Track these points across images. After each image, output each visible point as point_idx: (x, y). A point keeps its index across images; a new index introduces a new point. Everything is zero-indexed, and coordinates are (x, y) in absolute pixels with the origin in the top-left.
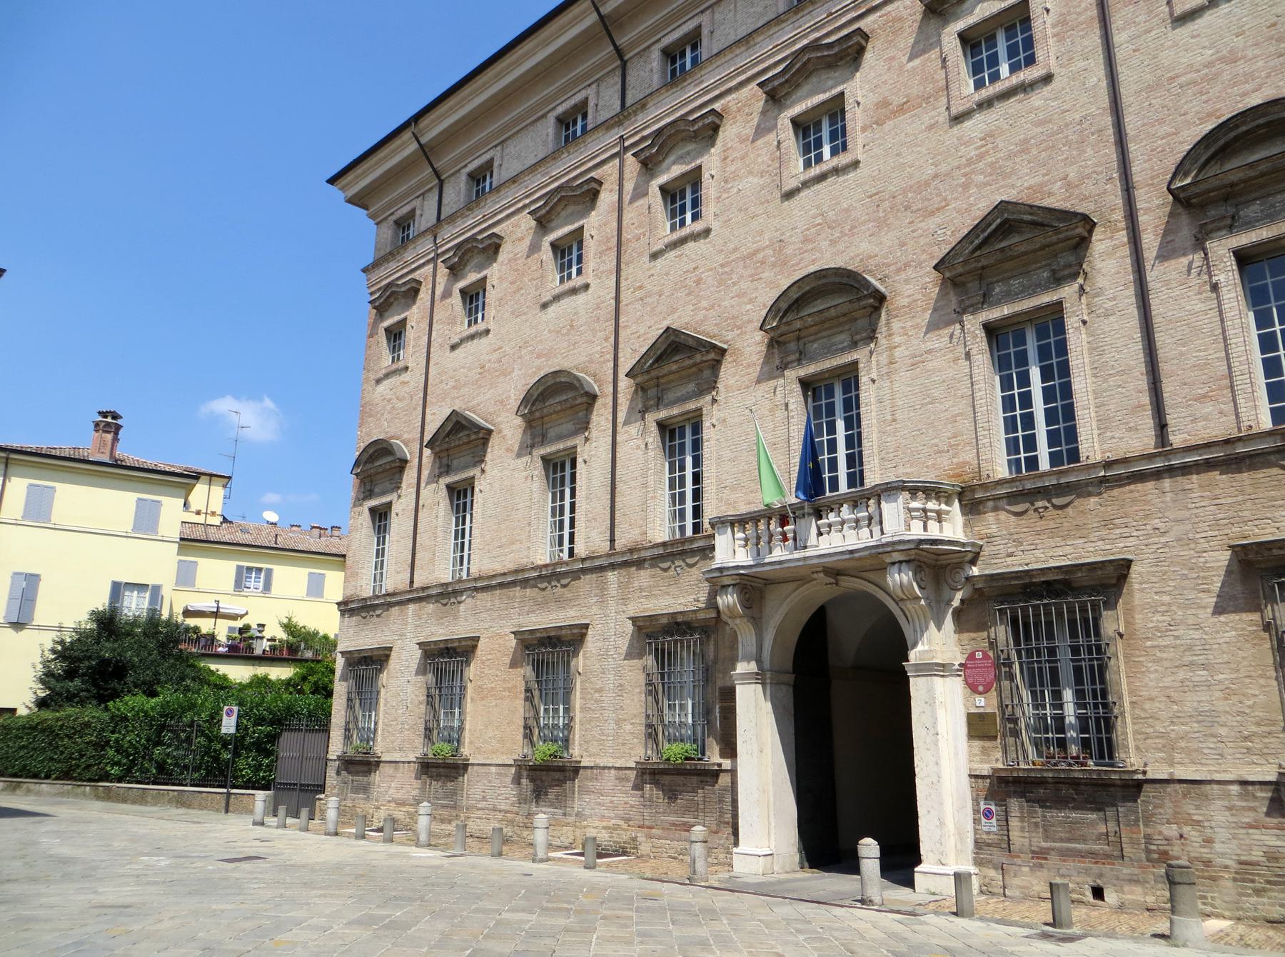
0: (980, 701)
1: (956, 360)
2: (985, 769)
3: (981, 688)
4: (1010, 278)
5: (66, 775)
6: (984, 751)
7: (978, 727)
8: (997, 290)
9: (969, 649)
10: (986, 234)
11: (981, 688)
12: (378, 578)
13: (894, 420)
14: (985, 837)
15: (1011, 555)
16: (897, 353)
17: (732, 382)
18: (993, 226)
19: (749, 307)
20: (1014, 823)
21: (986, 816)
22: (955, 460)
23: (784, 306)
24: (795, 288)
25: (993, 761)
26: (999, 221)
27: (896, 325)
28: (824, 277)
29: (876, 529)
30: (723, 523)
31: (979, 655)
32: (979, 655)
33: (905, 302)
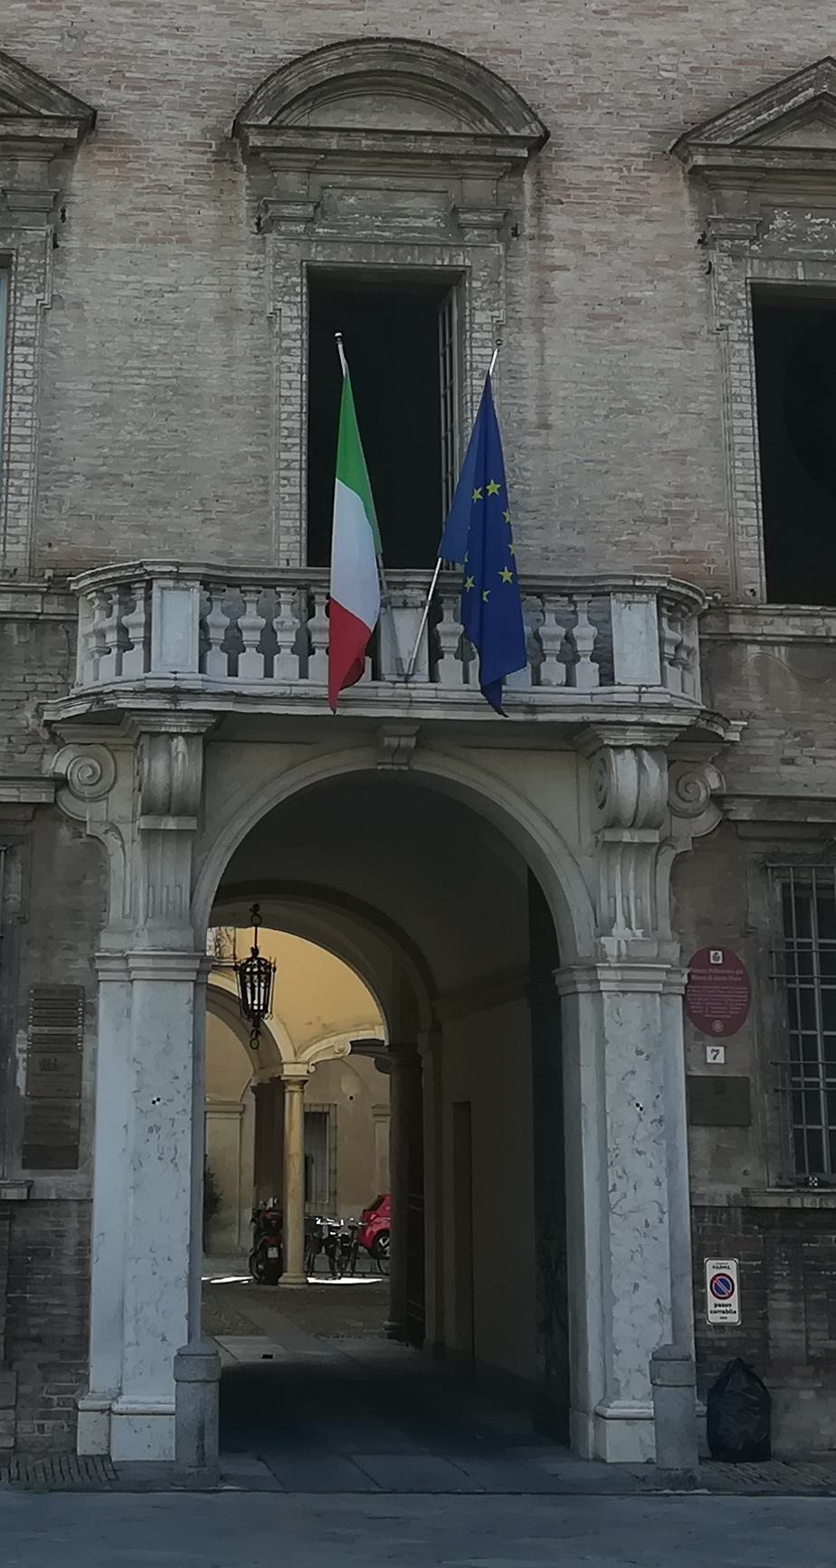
0: (716, 1055)
1: (689, 337)
2: (720, 1193)
3: (718, 1026)
4: (806, 207)
5: (769, 1413)
6: (720, 1159)
7: (711, 1101)
8: (779, 223)
9: (694, 945)
10: (785, 108)
11: (718, 1026)
12: (445, 634)
13: (546, 426)
14: (710, 1335)
15: (791, 761)
16: (559, 281)
17: (108, 213)
18: (800, 99)
19: (164, 44)
20: (780, 1304)
21: (718, 1293)
22: (678, 546)
23: (295, 84)
24: (333, 56)
25: (754, 1176)
26: (811, 91)
27: (558, 221)
28: (411, 58)
29: (587, 672)
30: (178, 577)
31: (716, 957)
32: (716, 957)
33: (583, 177)
